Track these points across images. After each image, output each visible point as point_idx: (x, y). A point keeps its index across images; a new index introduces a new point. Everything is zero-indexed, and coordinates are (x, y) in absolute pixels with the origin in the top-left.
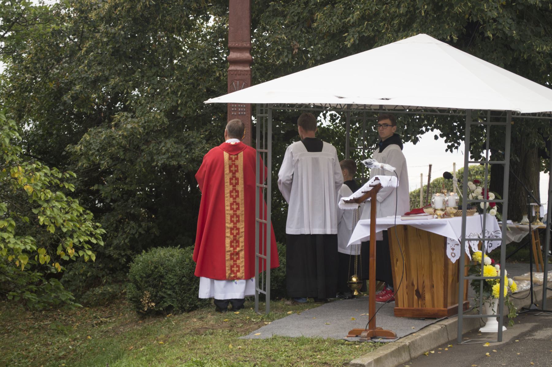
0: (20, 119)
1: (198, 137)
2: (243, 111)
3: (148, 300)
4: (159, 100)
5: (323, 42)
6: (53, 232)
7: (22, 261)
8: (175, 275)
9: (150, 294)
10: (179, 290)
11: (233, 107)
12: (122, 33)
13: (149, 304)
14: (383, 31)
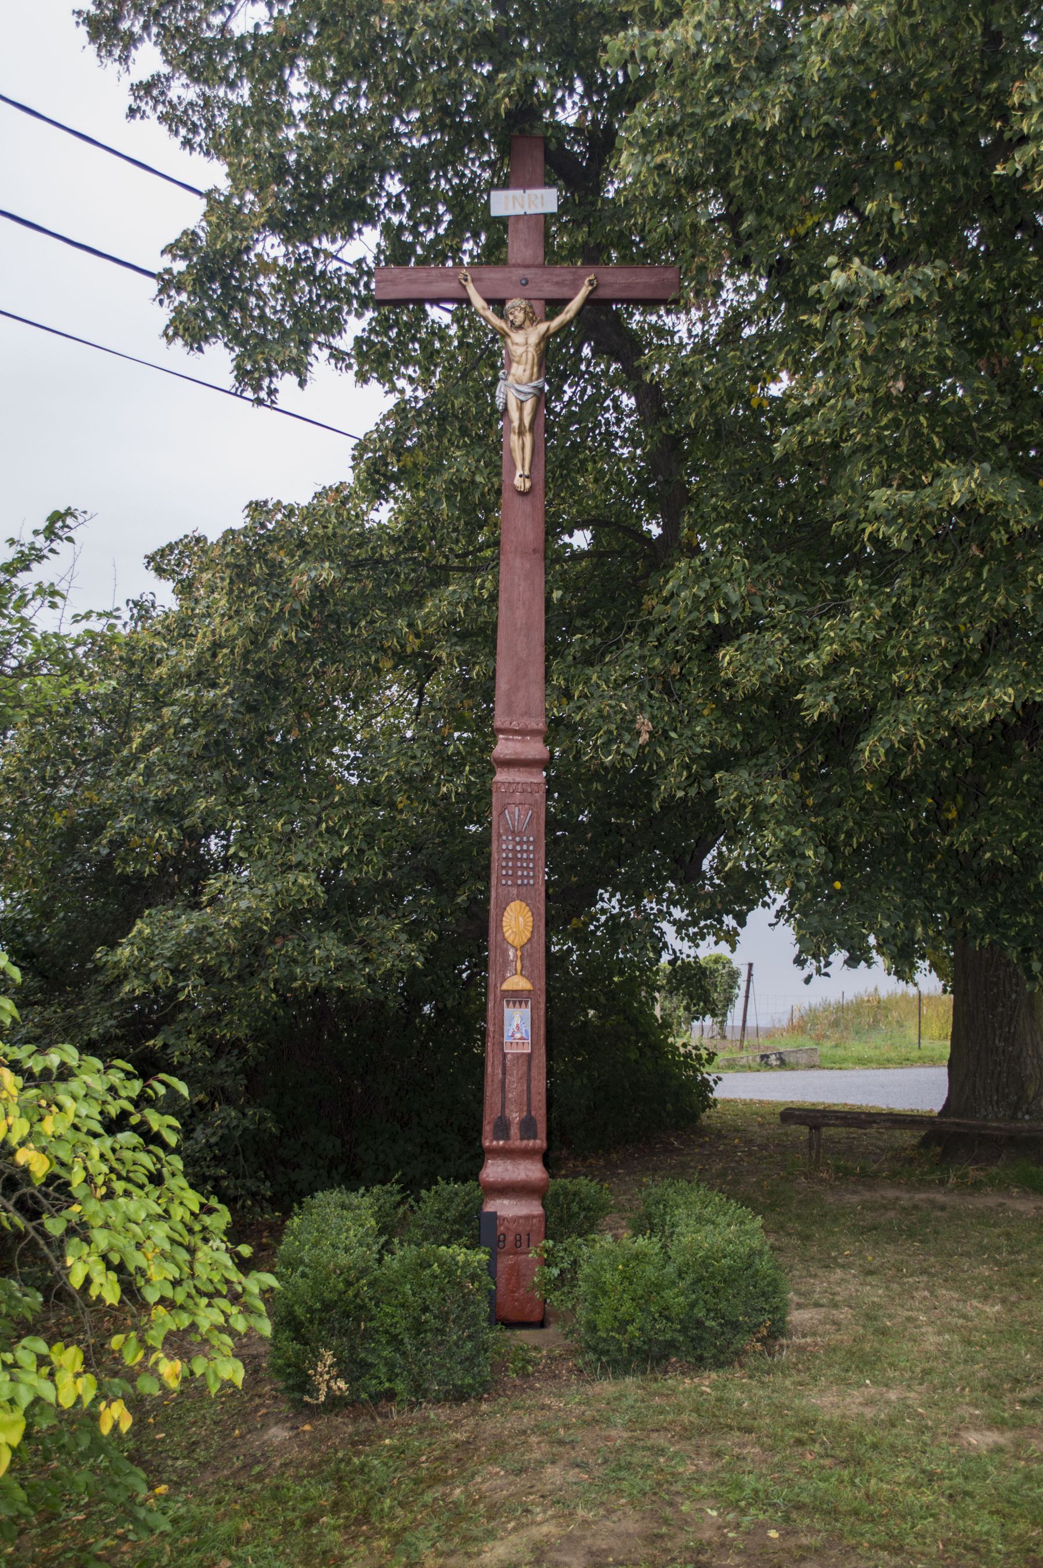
3: (328, 1372)
4: (302, 847)
6: (116, 1303)
8: (403, 1306)
9: (334, 1355)
12: (230, 701)
13: (332, 1383)
14: (909, 855)
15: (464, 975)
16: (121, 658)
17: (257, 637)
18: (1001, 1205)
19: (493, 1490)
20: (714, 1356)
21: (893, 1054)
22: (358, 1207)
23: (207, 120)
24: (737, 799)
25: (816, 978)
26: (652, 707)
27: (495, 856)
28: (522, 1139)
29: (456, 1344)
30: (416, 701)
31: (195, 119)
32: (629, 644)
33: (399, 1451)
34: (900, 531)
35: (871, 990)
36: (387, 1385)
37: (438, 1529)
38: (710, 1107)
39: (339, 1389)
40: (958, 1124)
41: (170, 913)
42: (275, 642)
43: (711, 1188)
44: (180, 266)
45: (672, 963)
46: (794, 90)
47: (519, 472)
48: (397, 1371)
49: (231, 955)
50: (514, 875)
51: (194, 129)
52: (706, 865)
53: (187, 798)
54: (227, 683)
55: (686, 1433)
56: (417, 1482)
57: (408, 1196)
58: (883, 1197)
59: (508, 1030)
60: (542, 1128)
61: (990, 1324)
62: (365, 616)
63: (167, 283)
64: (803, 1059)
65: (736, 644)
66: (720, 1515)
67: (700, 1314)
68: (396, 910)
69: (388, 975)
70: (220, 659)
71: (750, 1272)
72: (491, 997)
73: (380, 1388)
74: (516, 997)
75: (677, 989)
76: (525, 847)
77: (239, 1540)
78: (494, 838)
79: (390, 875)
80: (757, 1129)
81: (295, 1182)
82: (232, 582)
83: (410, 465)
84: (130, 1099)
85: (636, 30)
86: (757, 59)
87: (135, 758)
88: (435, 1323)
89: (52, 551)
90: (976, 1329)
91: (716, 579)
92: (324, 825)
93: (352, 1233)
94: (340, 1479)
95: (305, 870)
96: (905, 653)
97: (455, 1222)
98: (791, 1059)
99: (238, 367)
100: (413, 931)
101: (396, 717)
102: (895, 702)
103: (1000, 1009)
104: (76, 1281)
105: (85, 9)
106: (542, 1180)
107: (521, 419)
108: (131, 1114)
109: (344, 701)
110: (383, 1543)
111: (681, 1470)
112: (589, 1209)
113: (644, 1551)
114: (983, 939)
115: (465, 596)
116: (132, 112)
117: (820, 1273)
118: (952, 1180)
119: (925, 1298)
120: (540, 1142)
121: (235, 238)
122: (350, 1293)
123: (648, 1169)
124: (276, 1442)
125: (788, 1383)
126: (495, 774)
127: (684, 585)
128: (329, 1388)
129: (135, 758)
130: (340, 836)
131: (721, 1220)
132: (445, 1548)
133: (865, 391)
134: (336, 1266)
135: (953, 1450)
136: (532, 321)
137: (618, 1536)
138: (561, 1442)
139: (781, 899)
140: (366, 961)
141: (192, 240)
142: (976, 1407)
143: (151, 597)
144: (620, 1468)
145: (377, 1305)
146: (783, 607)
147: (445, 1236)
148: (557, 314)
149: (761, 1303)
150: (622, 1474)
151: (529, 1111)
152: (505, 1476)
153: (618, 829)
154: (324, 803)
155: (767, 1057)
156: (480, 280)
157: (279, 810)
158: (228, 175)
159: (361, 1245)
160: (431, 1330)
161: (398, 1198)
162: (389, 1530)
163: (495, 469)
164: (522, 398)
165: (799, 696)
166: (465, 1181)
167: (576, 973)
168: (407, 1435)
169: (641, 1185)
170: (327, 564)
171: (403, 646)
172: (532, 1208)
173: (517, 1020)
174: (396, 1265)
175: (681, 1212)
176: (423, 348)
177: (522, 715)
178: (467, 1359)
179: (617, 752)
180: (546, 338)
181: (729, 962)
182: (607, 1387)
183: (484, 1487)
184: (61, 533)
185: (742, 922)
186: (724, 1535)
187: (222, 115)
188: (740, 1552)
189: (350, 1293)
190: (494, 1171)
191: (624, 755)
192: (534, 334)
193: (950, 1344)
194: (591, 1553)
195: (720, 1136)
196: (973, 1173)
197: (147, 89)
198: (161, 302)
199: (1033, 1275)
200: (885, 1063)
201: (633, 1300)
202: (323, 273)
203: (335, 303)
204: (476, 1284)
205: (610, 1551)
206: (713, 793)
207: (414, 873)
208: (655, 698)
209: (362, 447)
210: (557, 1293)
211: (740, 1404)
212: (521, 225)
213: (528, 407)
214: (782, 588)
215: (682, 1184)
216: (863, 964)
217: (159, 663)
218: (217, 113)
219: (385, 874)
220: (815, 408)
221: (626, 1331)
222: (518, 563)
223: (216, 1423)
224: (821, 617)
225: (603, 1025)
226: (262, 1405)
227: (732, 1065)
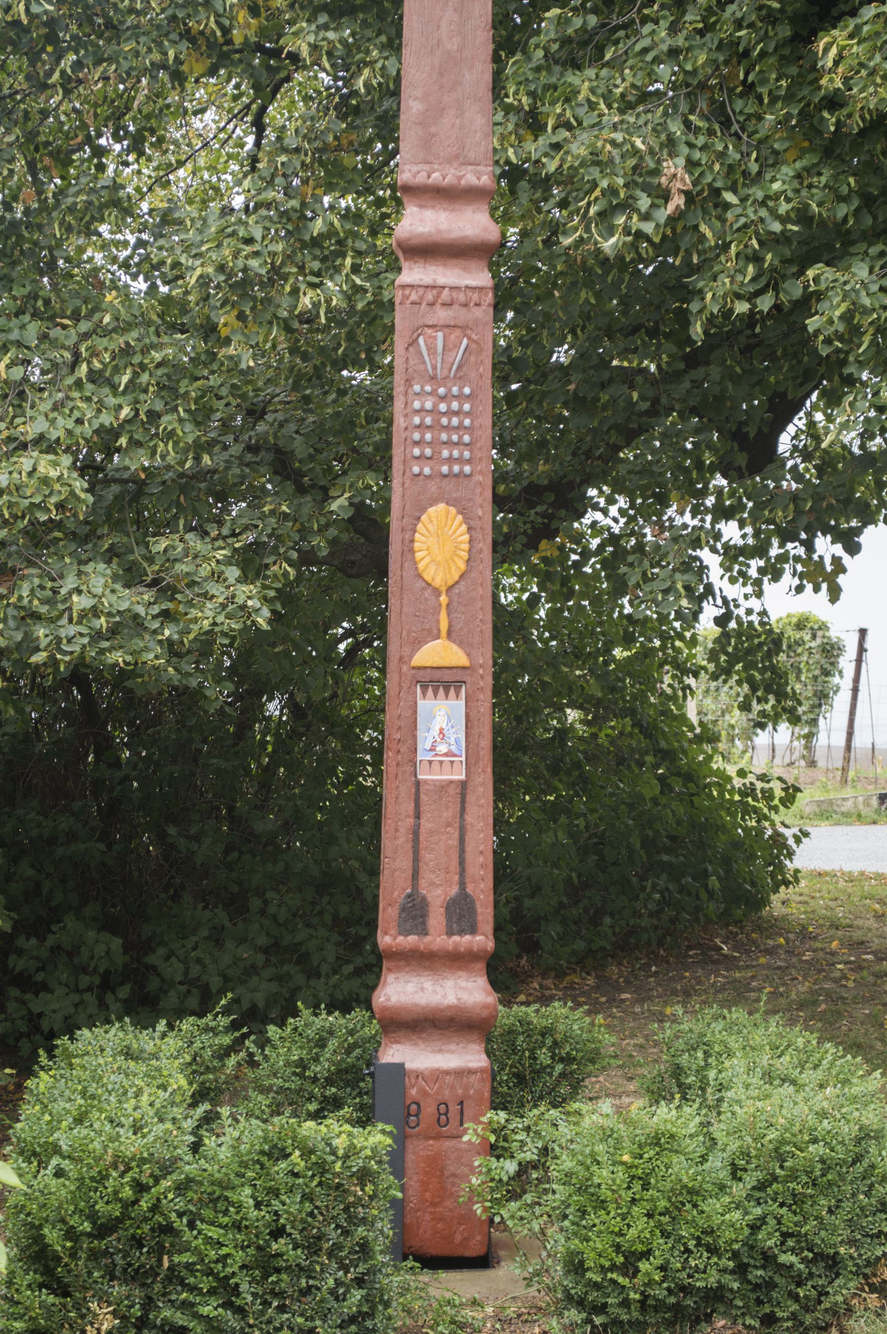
0: (182, 85)
1: (206, 559)
2: (460, 460)
4: (46, 406)
5: (791, 174)
8: (237, 1226)
10: (254, 1295)
11: (416, 443)
15: (342, 647)
20: (794, 1316)
22: (155, 1056)
24: (847, 317)
26: (691, 145)
27: (400, 422)
28: (450, 933)
29: (332, 1292)
30: (250, 140)
32: (648, 28)
38: (787, 883)
43: (792, 1022)
45: (721, 621)
50: (436, 454)
52: (784, 443)
57: (245, 1036)
59: (426, 738)
60: (485, 914)
65: (852, 23)
67: (768, 1240)
68: (220, 523)
69: (206, 642)
72: (391, 682)
75: (728, 672)
76: (455, 405)
78: (398, 390)
79: (206, 460)
81: (40, 1015)
88: (296, 1256)
92: (84, 367)
93: (145, 1099)
97: (329, 1081)
101: (212, 168)
106: (486, 1006)
109: (118, 139)
112: (568, 1060)
122: (144, 1205)
123: (675, 993)
126: (399, 270)
130: (114, 388)
131: (809, 1076)
140: (166, 615)
145: (191, 1225)
147: (313, 1107)
151: (462, 884)
153: (629, 377)
159: (161, 1120)
160: (288, 1269)
161: (227, 1040)
166: (346, 1009)
167: (546, 642)
169: (661, 1019)
171: (226, 31)
173: (440, 721)
174: (224, 1154)
175: (736, 1065)
177: (450, 161)
178: (352, 1319)
179: (627, 231)
181: (824, 627)
189: (144, 1205)
191: (640, 235)
195: (804, 935)
201: (649, 1215)
204: (369, 1188)
207: (249, 457)
208: (698, 130)
210: (513, 1205)
215: (738, 1014)
219: (197, 459)
221: (637, 1271)
225: (594, 736)
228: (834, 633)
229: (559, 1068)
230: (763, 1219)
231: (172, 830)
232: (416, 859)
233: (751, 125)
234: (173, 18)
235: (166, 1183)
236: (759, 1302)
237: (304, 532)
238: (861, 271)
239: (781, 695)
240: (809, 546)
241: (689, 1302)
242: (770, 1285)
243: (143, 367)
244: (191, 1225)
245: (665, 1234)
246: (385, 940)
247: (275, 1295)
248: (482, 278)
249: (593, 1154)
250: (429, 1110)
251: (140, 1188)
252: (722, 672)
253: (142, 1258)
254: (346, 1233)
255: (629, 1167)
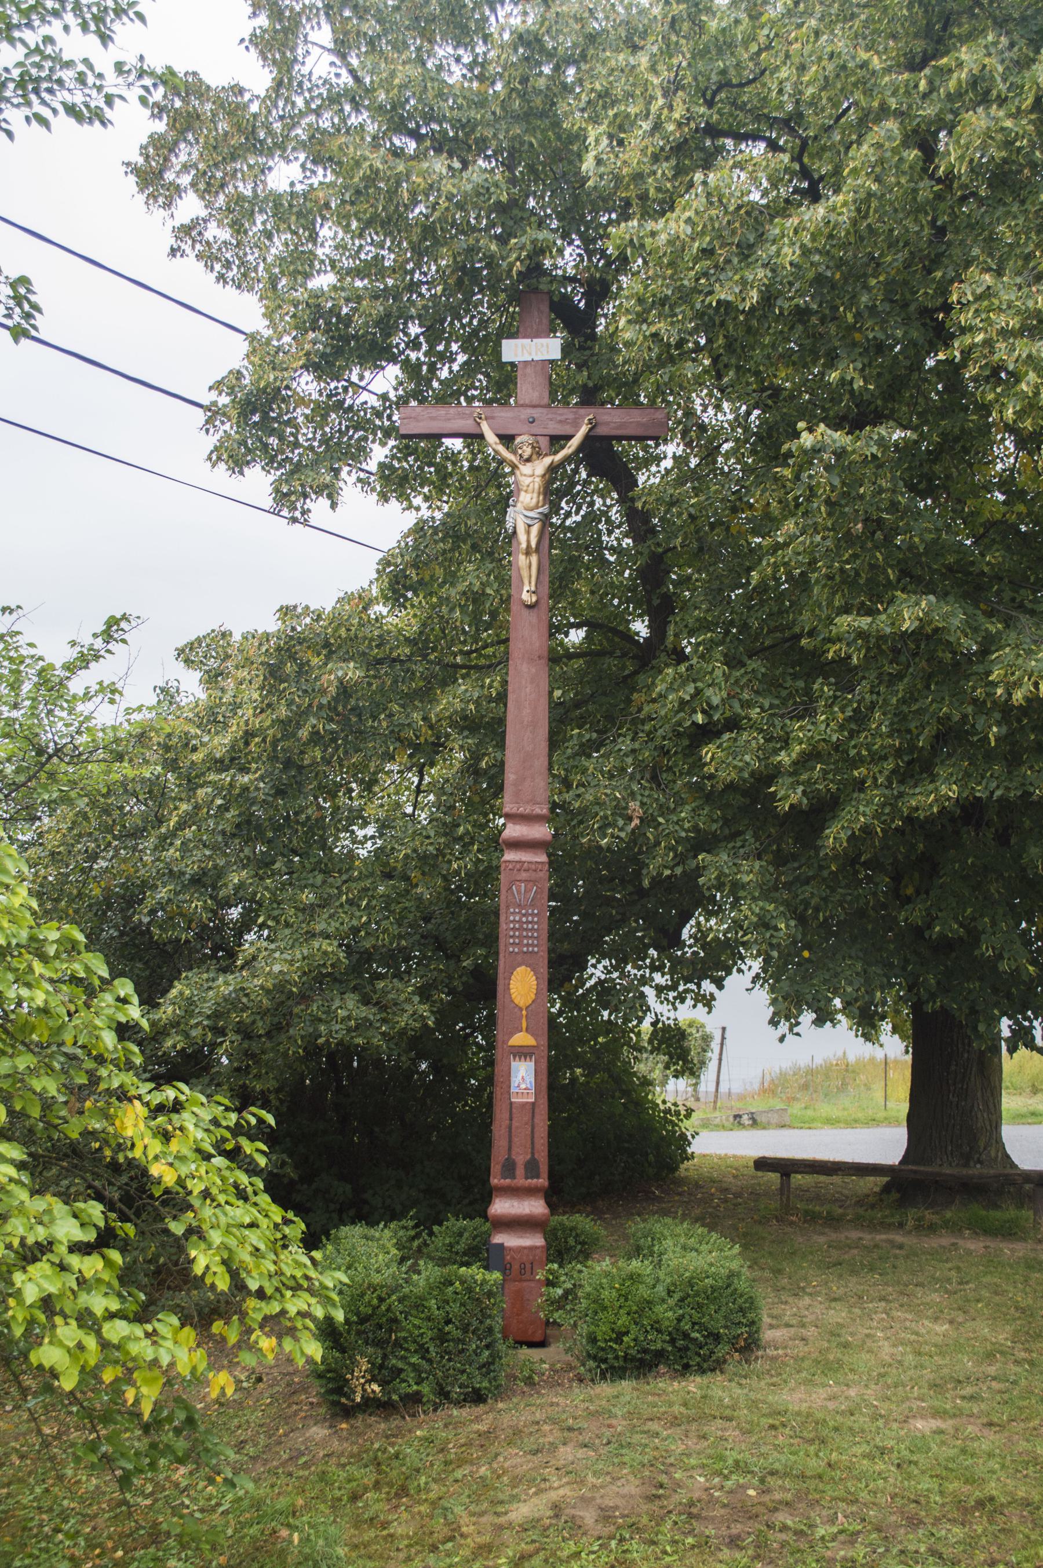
2: (533, 945)
4: (326, 916)
6: (226, 1289)
7: (144, 1390)
8: (429, 1319)
12: (262, 785)
13: (367, 1386)
16: (159, 744)
17: (288, 726)
18: (953, 1244)
19: (515, 1467)
20: (698, 1364)
21: (860, 1115)
23: (239, 258)
24: (718, 878)
25: (789, 1037)
28: (527, 1178)
29: (475, 1351)
31: (228, 256)
33: (429, 1441)
34: (859, 650)
35: (840, 1054)
36: (415, 1387)
37: (469, 1496)
38: (688, 1159)
39: (373, 1391)
40: (915, 1172)
41: (205, 976)
42: (304, 733)
44: (224, 400)
45: (654, 1024)
46: (770, 275)
47: (526, 588)
48: (424, 1375)
49: (263, 1013)
50: (521, 942)
51: (228, 265)
52: (685, 933)
53: (220, 873)
54: (258, 769)
55: (675, 1422)
56: (447, 1463)
58: (847, 1238)
60: (544, 1169)
61: (939, 1340)
62: (384, 710)
63: (213, 413)
64: (775, 1119)
65: (718, 742)
66: (707, 1480)
70: (252, 747)
71: (729, 1290)
73: (410, 1390)
74: (523, 1053)
77: (294, 1513)
80: (731, 1179)
82: (265, 679)
83: (427, 578)
84: (227, 1128)
85: (635, 223)
86: (738, 246)
87: (173, 834)
88: (457, 1334)
89: (109, 651)
90: (926, 1343)
91: (699, 684)
94: (379, 1464)
95: (328, 937)
96: (864, 753)
97: (465, 1254)
98: (761, 1119)
99: (277, 491)
100: (424, 993)
102: (855, 795)
103: (953, 1068)
104: (198, 1269)
105: (133, 161)
107: (528, 541)
108: (228, 1140)
110: (424, 1508)
111: (673, 1447)
112: (583, 1243)
113: (645, 1507)
114: (935, 1002)
115: (476, 695)
116: (173, 252)
117: (790, 1300)
118: (911, 1223)
119: (883, 1319)
120: (543, 1181)
121: (276, 379)
122: (383, 1308)
124: (318, 1438)
125: (763, 1383)
127: (670, 689)
128: (364, 1390)
129: (173, 834)
130: (359, 906)
131: (704, 1247)
132: (477, 1510)
133: (829, 530)
134: (370, 1285)
135: (902, 1433)
136: (539, 454)
137: (623, 1497)
138: (570, 1429)
139: (756, 965)
140: (384, 1021)
141: (237, 379)
142: (923, 1401)
143: (176, 684)
144: (622, 1446)
145: (406, 1319)
146: (758, 710)
148: (563, 447)
149: (738, 1317)
150: (623, 1451)
151: (533, 1154)
152: (524, 1456)
154: (344, 877)
155: (740, 1116)
156: (493, 418)
157: (303, 882)
158: (264, 315)
160: (453, 1340)
161: (412, 1233)
162: (426, 1500)
163: (504, 582)
164: (529, 522)
165: (772, 789)
168: (433, 1428)
170: (352, 665)
172: (535, 1240)
174: (422, 1283)
175: (669, 1243)
176: (437, 472)
178: (484, 1366)
180: (552, 469)
181: (703, 1026)
182: (606, 1389)
183: (506, 1465)
184: (116, 636)
185: (719, 984)
186: (712, 1495)
187: (253, 253)
188: (725, 1506)
189: (383, 1308)
190: (501, 1207)
192: (540, 466)
193: (902, 1354)
194: (602, 1509)
195: (697, 1185)
196: (929, 1216)
197: (188, 231)
198: (207, 431)
199: (978, 1301)
200: (852, 1123)
201: (628, 1314)
202: (351, 407)
203: (361, 433)
205: (616, 1508)
206: (699, 871)
209: (385, 562)
211: (721, 1400)
212: (529, 370)
213: (535, 530)
214: (757, 692)
215: (668, 1220)
216: (828, 1023)
217: (195, 749)
218: (248, 250)
220: (786, 545)
222: (524, 668)
223: (261, 1426)
224: (791, 719)
226: (301, 1410)
227: (706, 1124)
228: (708, 1030)
229: (579, 1247)
230: (683, 1316)
231: (377, 1129)
232: (510, 1141)
233: (671, 785)
234: (392, 732)
235: (394, 1297)
236: (681, 1357)
237: (450, 978)
238: (724, 857)
239: (686, 1061)
240: (699, 986)
241: (648, 1357)
242: (686, 1349)
243: (373, 897)
244: (406, 1319)
245: (636, 1324)
246: (494, 1181)
247: (447, 1353)
248: (543, 858)
249: (601, 1284)
250: (516, 1267)
251: (381, 1300)
252: (656, 1050)
253: (382, 1334)
254: (481, 1322)
255: (618, 1290)
